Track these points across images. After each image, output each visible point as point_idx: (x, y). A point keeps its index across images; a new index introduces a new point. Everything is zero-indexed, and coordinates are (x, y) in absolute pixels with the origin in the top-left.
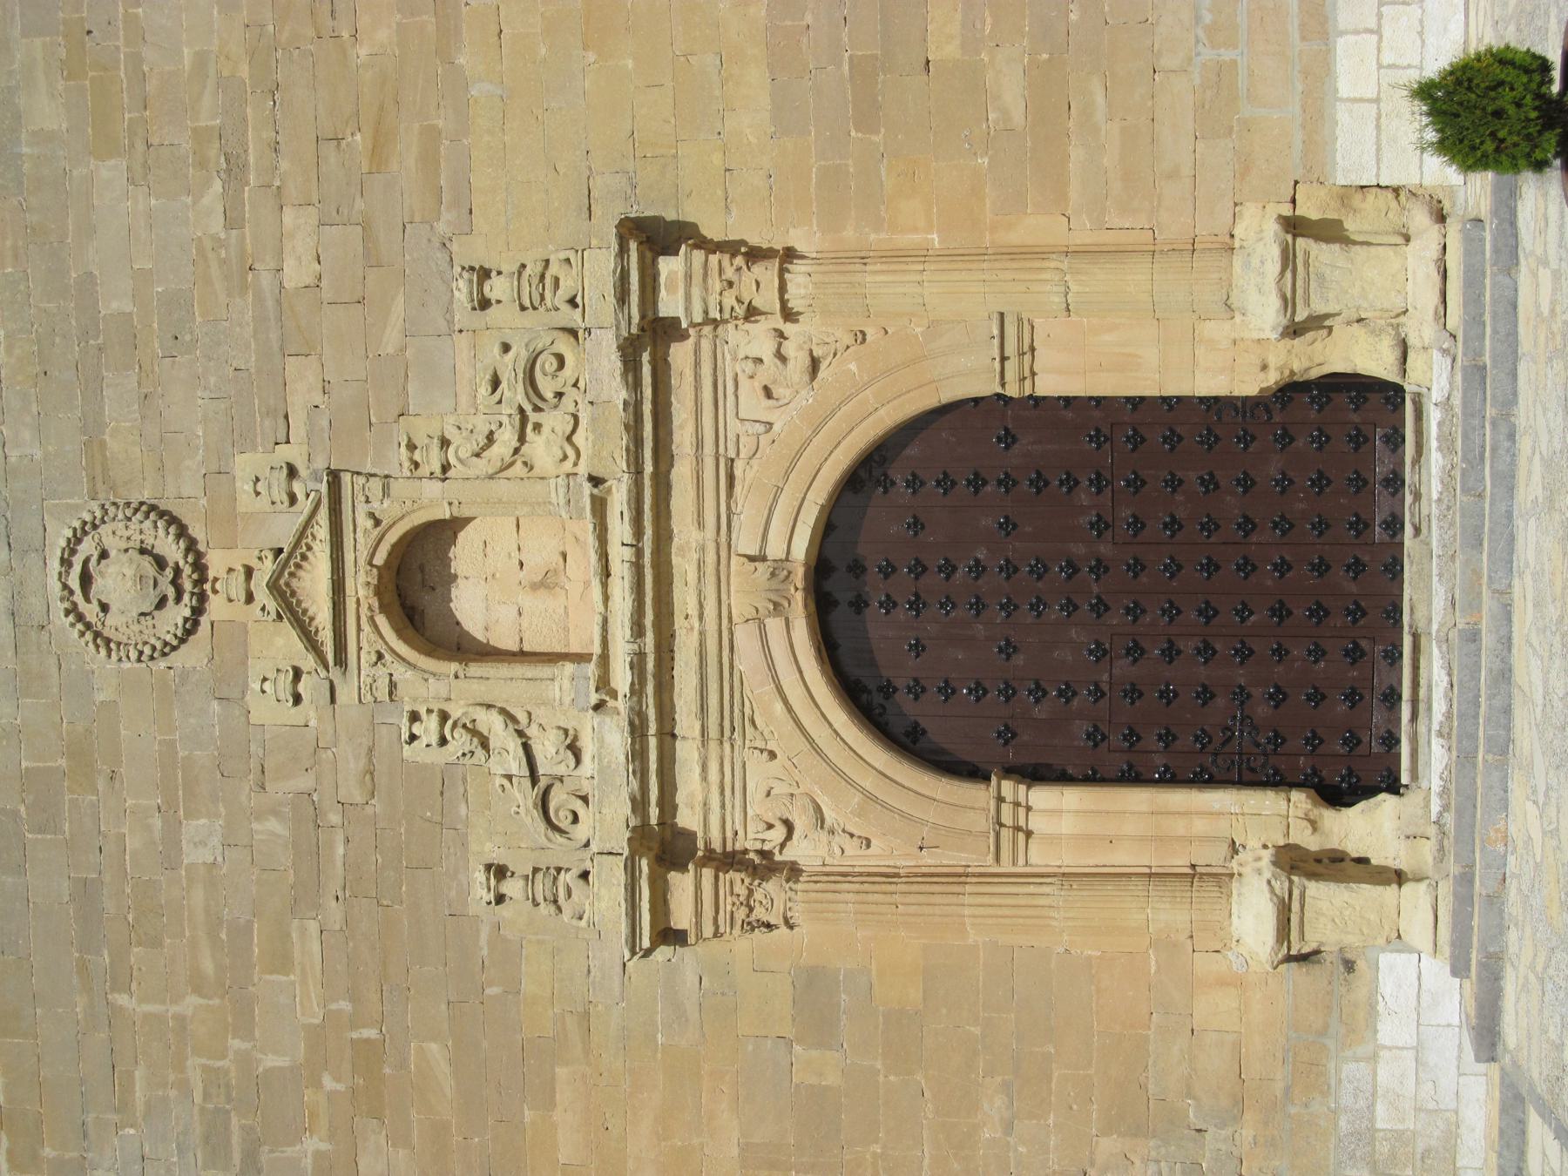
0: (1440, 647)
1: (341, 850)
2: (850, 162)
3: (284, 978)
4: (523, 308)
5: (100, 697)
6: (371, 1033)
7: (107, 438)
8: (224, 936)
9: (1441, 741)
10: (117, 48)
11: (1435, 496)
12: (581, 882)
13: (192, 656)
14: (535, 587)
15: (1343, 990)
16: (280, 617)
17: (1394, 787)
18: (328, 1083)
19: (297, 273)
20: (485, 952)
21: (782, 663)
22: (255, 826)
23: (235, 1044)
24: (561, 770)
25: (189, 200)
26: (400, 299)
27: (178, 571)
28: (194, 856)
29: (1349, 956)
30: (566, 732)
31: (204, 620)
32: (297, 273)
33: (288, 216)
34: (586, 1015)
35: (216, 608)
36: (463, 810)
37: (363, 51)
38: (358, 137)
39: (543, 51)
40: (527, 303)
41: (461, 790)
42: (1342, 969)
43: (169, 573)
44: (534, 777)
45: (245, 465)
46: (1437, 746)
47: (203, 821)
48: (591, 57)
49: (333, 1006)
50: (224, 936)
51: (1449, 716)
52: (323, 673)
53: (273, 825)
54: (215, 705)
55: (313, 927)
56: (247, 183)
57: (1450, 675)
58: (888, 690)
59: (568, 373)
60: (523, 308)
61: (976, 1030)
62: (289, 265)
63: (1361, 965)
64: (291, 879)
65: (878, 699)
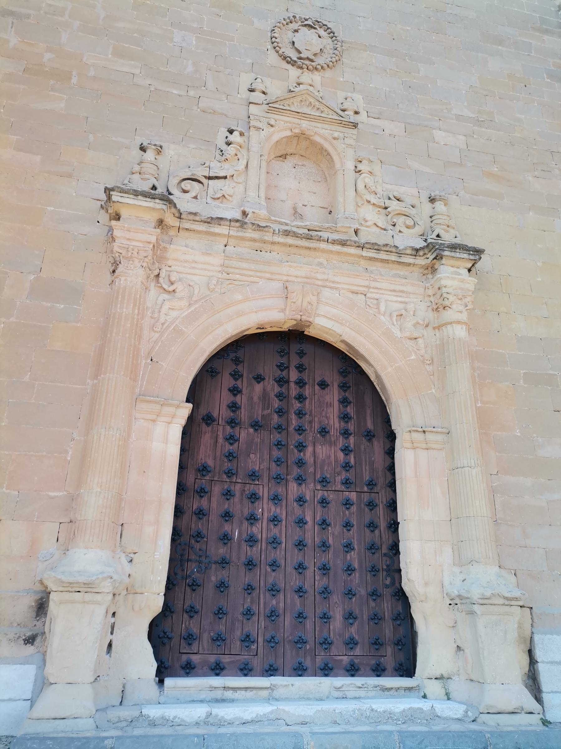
0: (272, 712)
1: (175, 92)
2: (509, 368)
3: (110, 52)
4: (431, 217)
5: (255, 20)
6: (74, 80)
7: (368, 52)
8: (135, 35)
9: (204, 715)
10: (521, 94)
11: (374, 707)
12: (151, 186)
13: (272, 58)
14: (295, 209)
15: (11, 636)
16: (290, 91)
17: (162, 673)
18: (48, 56)
19: (438, 134)
20: (114, 139)
21: (260, 310)
22: (190, 62)
23: (77, 24)
24: (211, 191)
25: (466, 104)
26: (432, 172)
27: (312, 61)
28: (178, 35)
29: (38, 639)
30: (231, 196)
31: (289, 67)
32: (438, 134)
33: (462, 137)
34: (70, 176)
35: (294, 72)
36: (192, 146)
37: (530, 178)
38: (496, 169)
39: (540, 246)
40: (433, 218)
41: (203, 148)
42: (29, 634)
43: (312, 57)
44: (210, 178)
45: (358, 97)
46: (199, 712)
47: (194, 42)
48: (540, 264)
49: (92, 69)
50: (135, 35)
51: (221, 723)
52: (265, 102)
53: (190, 69)
54: (249, 61)
55: (137, 71)
56: (474, 126)
57: (252, 722)
58: (237, 361)
59: (404, 229)
60: (431, 217)
61: (26, 379)
62: (444, 134)
63: (30, 649)
64: (162, 69)
65: (232, 355)
